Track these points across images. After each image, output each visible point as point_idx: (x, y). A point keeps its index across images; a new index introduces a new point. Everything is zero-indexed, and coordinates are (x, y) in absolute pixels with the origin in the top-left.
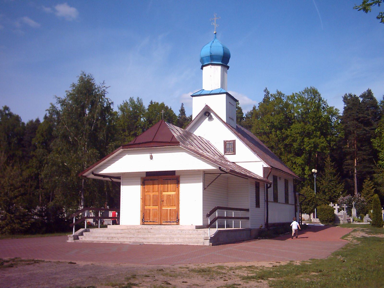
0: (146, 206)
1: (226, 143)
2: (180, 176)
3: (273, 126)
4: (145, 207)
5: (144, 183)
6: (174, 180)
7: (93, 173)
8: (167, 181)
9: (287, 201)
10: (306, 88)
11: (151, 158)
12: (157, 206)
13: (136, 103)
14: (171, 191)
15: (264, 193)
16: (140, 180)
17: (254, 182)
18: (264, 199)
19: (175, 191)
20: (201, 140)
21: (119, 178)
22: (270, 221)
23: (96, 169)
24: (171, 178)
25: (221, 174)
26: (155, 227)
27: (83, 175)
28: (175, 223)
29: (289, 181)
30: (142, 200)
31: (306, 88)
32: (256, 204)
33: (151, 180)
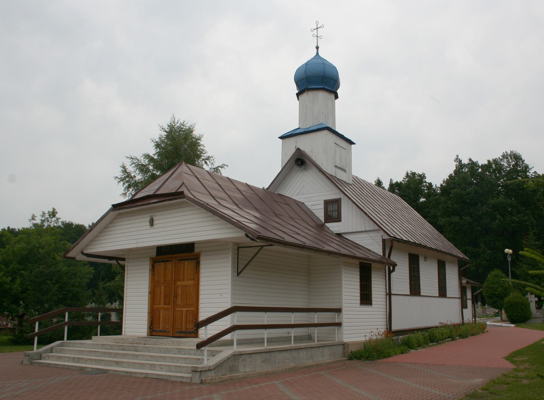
0: (156, 304)
1: (327, 203)
2: (200, 253)
4: (154, 306)
7: (82, 253)
8: (183, 262)
9: (443, 293)
11: (152, 223)
12: (169, 304)
15: (385, 280)
16: (148, 263)
17: (358, 263)
18: (385, 290)
19: (193, 280)
20: (429, 239)
24: (187, 258)
26: (150, 341)
28: (193, 335)
29: (446, 262)
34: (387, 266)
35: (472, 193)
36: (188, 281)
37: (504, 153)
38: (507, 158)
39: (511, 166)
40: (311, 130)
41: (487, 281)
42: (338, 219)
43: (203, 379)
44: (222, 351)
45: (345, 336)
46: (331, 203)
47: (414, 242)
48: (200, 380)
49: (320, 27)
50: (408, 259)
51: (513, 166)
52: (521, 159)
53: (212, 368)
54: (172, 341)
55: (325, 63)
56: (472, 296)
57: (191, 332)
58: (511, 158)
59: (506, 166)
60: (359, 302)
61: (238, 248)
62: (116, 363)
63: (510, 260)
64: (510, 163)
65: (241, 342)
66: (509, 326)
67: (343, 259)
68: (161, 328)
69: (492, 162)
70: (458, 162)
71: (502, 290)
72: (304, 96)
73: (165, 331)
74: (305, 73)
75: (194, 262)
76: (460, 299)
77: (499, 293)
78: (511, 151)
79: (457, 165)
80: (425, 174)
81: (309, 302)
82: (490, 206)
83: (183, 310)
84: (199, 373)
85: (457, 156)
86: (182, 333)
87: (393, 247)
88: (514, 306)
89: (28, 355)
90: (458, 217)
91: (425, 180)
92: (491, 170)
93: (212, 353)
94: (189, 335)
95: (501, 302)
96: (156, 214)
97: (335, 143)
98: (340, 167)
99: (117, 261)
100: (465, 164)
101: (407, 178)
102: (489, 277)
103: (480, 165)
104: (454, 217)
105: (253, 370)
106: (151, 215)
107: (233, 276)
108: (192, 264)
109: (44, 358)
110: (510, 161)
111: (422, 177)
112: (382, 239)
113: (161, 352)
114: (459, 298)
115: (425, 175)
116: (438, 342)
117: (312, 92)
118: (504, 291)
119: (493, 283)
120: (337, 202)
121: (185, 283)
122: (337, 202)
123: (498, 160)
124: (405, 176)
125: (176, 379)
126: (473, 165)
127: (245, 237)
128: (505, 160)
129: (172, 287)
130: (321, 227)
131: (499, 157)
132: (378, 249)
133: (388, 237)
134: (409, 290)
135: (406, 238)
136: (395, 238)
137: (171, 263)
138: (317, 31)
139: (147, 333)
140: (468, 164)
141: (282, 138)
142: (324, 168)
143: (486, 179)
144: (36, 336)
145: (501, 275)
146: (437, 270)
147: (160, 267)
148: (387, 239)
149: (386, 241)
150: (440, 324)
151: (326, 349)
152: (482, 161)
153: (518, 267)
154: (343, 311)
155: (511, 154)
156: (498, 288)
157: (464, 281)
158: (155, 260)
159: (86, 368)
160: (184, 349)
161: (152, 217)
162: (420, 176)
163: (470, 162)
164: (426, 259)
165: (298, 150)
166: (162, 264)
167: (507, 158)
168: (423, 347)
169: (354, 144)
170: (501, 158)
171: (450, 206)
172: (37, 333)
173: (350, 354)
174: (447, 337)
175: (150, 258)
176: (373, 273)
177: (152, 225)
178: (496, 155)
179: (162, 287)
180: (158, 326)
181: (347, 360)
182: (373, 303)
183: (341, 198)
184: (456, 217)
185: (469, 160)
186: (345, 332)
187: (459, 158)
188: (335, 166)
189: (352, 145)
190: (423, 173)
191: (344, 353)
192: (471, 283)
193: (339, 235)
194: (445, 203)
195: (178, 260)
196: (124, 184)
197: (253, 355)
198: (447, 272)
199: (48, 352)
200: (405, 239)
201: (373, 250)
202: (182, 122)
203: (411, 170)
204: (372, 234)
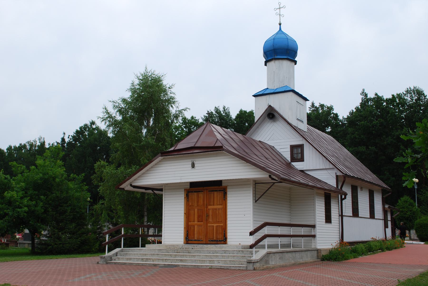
0: (191, 222)
1: (292, 147)
3: (147, 71)
4: (189, 223)
5: (188, 195)
6: (220, 192)
7: (131, 185)
8: (213, 192)
9: (372, 216)
10: (408, 88)
11: (193, 166)
12: (202, 222)
13: (222, 112)
14: (217, 205)
16: (183, 193)
17: (324, 193)
18: (338, 212)
19: (222, 205)
21: (161, 190)
22: (346, 240)
23: (135, 180)
25: (274, 183)
26: (197, 246)
27: (120, 187)
28: (223, 242)
30: (185, 215)
31: (408, 88)
32: (326, 219)
33: (196, 192)
34: (340, 195)
35: (378, 125)
36: (217, 205)
37: (407, 88)
38: (411, 93)
39: (414, 100)
40: (282, 91)
41: (398, 205)
42: (302, 160)
43: (255, 267)
44: (259, 251)
45: (318, 244)
46: (295, 147)
47: (357, 177)
48: (253, 268)
49: (282, 7)
50: (351, 189)
51: (416, 100)
52: (424, 94)
53: (258, 261)
54: (215, 246)
55: (287, 38)
56: (391, 218)
57: (221, 240)
58: (414, 93)
59: (410, 100)
60: (324, 221)
61: (256, 183)
62: (181, 261)
63: (417, 188)
64: (413, 98)
65: (270, 247)
66: (420, 243)
67: (315, 190)
68: (196, 238)
69: (396, 97)
70: (364, 96)
71: (411, 214)
72: (271, 64)
73: (199, 240)
74: (273, 46)
75: (222, 193)
76: (383, 221)
77: (408, 216)
78: (414, 87)
79: (363, 98)
80: (333, 106)
81: (291, 221)
82: (394, 137)
83: (214, 226)
84: (252, 264)
85: (364, 90)
86: (213, 241)
87: (345, 182)
88: (423, 227)
89: (104, 258)
90: (365, 147)
91: (333, 111)
92: (395, 104)
93: (251, 253)
94: (219, 243)
95: (410, 224)
96: (196, 160)
97: (297, 102)
98: (300, 119)
99: (152, 191)
100: (371, 98)
101: (312, 107)
102: (399, 202)
103: (385, 99)
104: (361, 147)
105: (276, 264)
106: (193, 160)
107: (253, 203)
108: (221, 194)
109: (114, 260)
110: (413, 96)
111: (330, 109)
112: (335, 175)
113: (210, 253)
114: (383, 219)
115: (333, 107)
116: (373, 252)
117: (278, 61)
118: (412, 214)
119: (403, 208)
120: (301, 147)
121: (215, 207)
122: (301, 147)
123: (402, 95)
124: (310, 106)
125: (235, 268)
126: (378, 99)
127: (269, 178)
128: (408, 95)
129: (204, 210)
130: (289, 165)
131: (403, 93)
132: (333, 182)
133: (341, 174)
134: (352, 212)
135: (352, 174)
136: (346, 174)
137: (202, 193)
138: (280, 10)
139: (183, 242)
140: (374, 98)
141: (254, 96)
142: (290, 121)
143: (390, 112)
144: (107, 244)
145: (410, 201)
146: (368, 197)
147: (194, 196)
148: (340, 176)
149: (338, 176)
150: (372, 239)
151: (309, 253)
152: (387, 96)
153: (422, 193)
154: (317, 226)
155: (414, 90)
156: (407, 212)
157: (387, 206)
158: (189, 191)
159: (158, 264)
160: (229, 251)
161: (193, 162)
162: (328, 108)
163: (376, 96)
164: (362, 189)
165: (270, 106)
166: (195, 194)
167: (411, 93)
168: (365, 255)
169: (308, 100)
170: (405, 93)
171: (357, 136)
172: (107, 242)
173: (322, 256)
174: (379, 249)
175: (185, 190)
176: (332, 200)
177: (193, 167)
178: (401, 90)
179: (196, 210)
180: (193, 237)
181: (320, 261)
182: (332, 221)
183: (304, 144)
184: (363, 146)
185: (375, 94)
186: (318, 242)
187: (365, 92)
188: (297, 119)
189: (307, 101)
190: (331, 105)
191: (318, 256)
192: (391, 208)
193: (302, 171)
194: (353, 134)
195: (209, 191)
196: (106, 123)
197: (275, 254)
198: (375, 199)
199: (114, 256)
200: (352, 175)
201: (328, 183)
202: (153, 72)
203: (320, 103)
204: (330, 171)
